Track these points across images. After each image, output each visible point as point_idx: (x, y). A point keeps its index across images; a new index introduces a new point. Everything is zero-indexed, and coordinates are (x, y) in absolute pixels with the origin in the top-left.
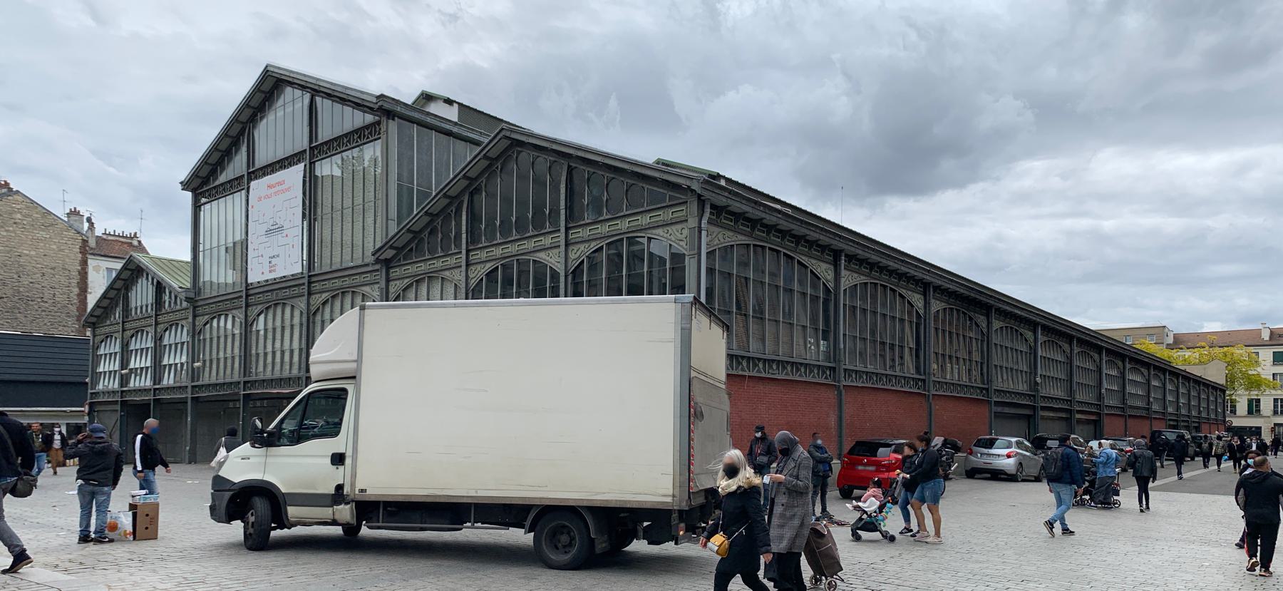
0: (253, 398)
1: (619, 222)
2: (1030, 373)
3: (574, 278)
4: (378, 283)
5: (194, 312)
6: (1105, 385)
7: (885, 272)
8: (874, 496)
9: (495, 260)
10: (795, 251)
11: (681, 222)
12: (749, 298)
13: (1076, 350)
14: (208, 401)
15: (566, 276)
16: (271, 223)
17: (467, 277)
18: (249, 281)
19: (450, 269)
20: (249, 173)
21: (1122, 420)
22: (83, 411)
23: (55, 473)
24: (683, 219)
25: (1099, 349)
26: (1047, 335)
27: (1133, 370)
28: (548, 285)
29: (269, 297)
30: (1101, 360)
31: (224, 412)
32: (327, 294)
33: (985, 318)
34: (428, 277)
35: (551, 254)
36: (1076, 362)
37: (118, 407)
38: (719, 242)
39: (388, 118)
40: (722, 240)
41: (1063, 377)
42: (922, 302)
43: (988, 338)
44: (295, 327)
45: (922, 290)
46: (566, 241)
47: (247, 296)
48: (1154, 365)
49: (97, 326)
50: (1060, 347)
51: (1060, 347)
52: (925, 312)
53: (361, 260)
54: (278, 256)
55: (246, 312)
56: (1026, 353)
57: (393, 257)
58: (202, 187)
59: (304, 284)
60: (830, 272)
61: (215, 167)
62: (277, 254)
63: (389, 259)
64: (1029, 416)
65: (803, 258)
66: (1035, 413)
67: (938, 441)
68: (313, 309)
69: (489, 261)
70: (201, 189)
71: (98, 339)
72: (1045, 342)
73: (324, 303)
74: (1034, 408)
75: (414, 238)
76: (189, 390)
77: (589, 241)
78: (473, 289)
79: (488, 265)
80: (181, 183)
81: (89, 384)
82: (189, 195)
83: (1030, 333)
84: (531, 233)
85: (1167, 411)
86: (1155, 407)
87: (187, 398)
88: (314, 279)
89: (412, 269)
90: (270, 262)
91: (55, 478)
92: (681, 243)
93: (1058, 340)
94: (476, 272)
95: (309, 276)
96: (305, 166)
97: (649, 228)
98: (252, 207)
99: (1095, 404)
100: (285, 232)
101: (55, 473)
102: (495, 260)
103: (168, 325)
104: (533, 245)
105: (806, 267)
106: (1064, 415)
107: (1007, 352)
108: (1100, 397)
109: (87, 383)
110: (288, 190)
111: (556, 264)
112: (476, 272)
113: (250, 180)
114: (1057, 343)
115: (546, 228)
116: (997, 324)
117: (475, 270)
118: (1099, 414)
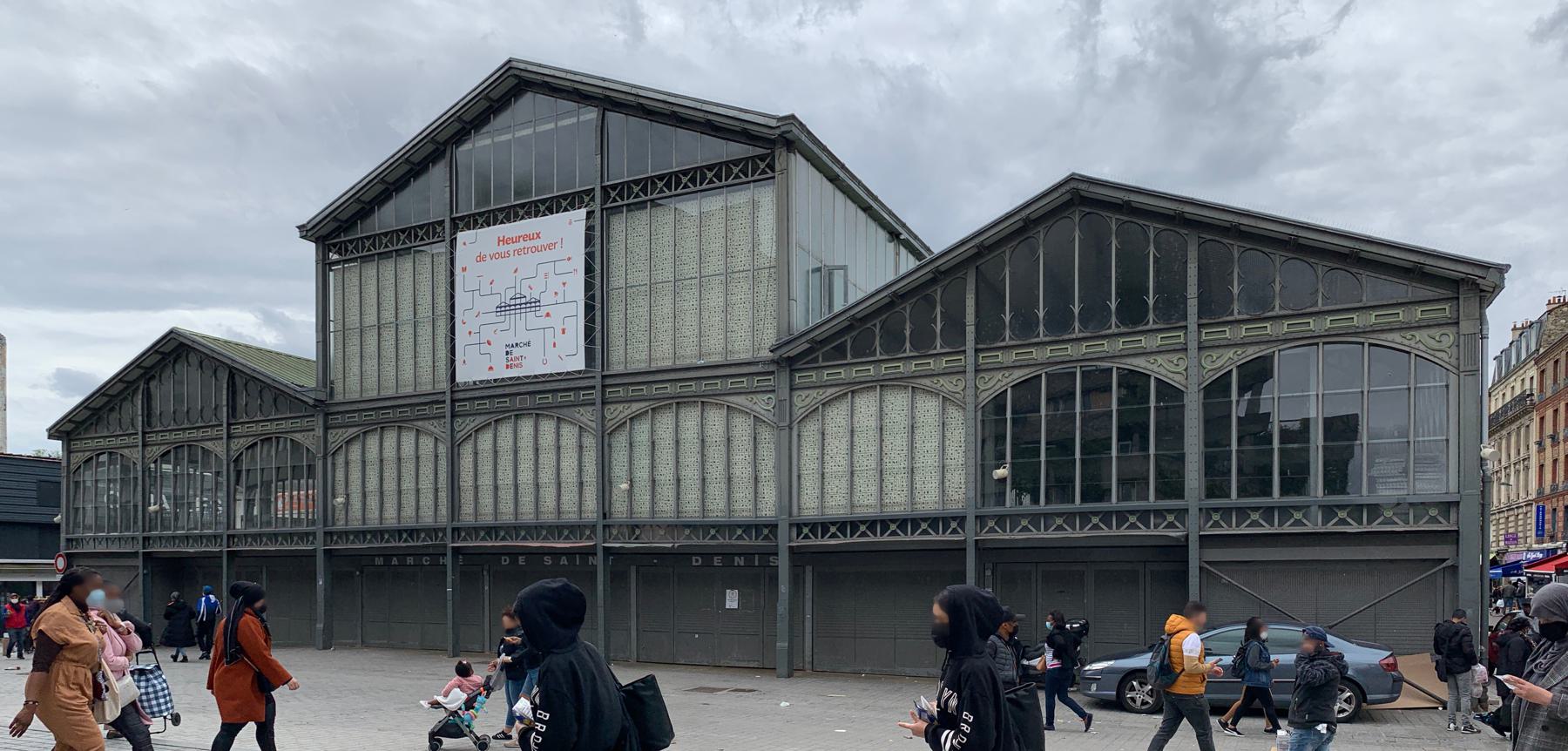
0: (464, 552)
1: (1033, 350)
3: (236, 466)
4: (313, 430)
5: (325, 422)
8: (459, 687)
9: (167, 443)
11: (958, 373)
14: (355, 557)
15: (228, 465)
16: (511, 293)
17: (453, 429)
18: (458, 379)
19: (128, 447)
20: (453, 220)
22: (53, 564)
24: (961, 369)
28: (1152, 404)
29: (99, 444)
31: (362, 572)
32: (355, 429)
34: (881, 386)
35: (755, 400)
37: (139, 562)
38: (961, 399)
39: (789, 151)
44: (352, 465)
46: (452, 413)
47: (453, 401)
49: (72, 437)
53: (395, 390)
54: (528, 344)
55: (452, 425)
57: (72, 430)
58: (338, 236)
59: (593, 387)
61: (368, 207)
62: (526, 341)
63: (792, 358)
68: (610, 425)
69: (164, 444)
70: (334, 238)
71: (78, 458)
73: (349, 442)
75: (93, 415)
76: (320, 536)
77: (1243, 344)
78: (983, 407)
79: (163, 448)
80: (300, 228)
81: (63, 526)
82: (310, 248)
84: (1114, 330)
87: (315, 550)
88: (609, 381)
89: (92, 444)
90: (507, 353)
91: (21, 661)
92: (957, 395)
94: (463, 425)
95: (604, 377)
96: (590, 215)
97: (1374, 332)
98: (464, 269)
100: (544, 311)
102: (167, 443)
103: (257, 440)
104: (1286, 330)
109: (58, 526)
110: (551, 246)
111: (442, 434)
112: (463, 425)
113: (455, 228)
115: (1110, 327)
117: (336, 435)
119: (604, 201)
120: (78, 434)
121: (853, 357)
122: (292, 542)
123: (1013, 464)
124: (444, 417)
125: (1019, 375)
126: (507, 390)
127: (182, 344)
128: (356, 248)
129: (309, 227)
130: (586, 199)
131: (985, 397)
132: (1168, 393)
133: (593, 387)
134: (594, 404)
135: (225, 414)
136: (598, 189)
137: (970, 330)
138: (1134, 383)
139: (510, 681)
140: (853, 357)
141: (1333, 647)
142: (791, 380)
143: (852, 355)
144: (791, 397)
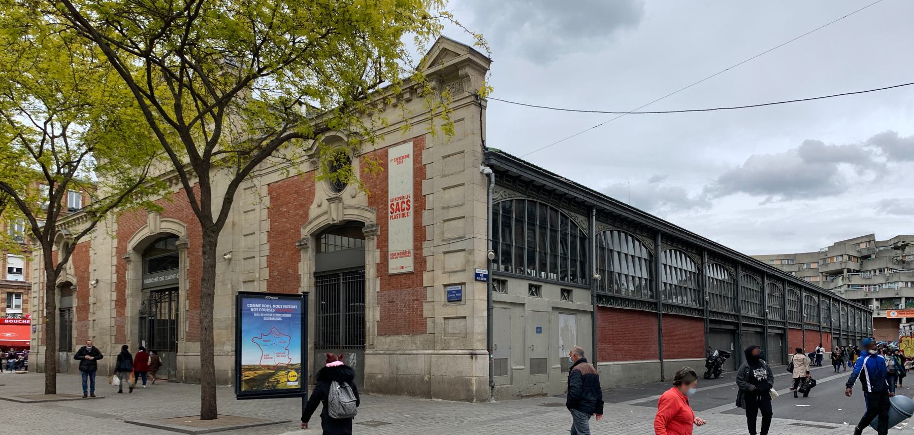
2: (699, 291)
6: (788, 307)
7: (625, 222)
10: (558, 207)
12: (567, 250)
13: (767, 282)
21: (654, 321)
23: (51, 389)
25: (762, 274)
26: (769, 280)
27: (791, 291)
30: (763, 282)
33: (586, 219)
36: (787, 297)
40: (504, 197)
41: (758, 303)
42: (701, 261)
43: (656, 258)
45: (585, 212)
48: (822, 294)
50: (755, 280)
51: (755, 280)
52: (589, 232)
56: (731, 284)
60: (584, 222)
64: (837, 338)
65: (565, 211)
66: (764, 330)
67: (716, 353)
72: (744, 275)
74: (737, 325)
83: (733, 269)
85: (740, 313)
86: (824, 324)
93: (725, 264)
99: (733, 315)
101: (51, 389)
105: (567, 218)
106: (759, 330)
107: (724, 284)
108: (764, 314)
114: (753, 277)
116: (804, 294)
118: (784, 329)
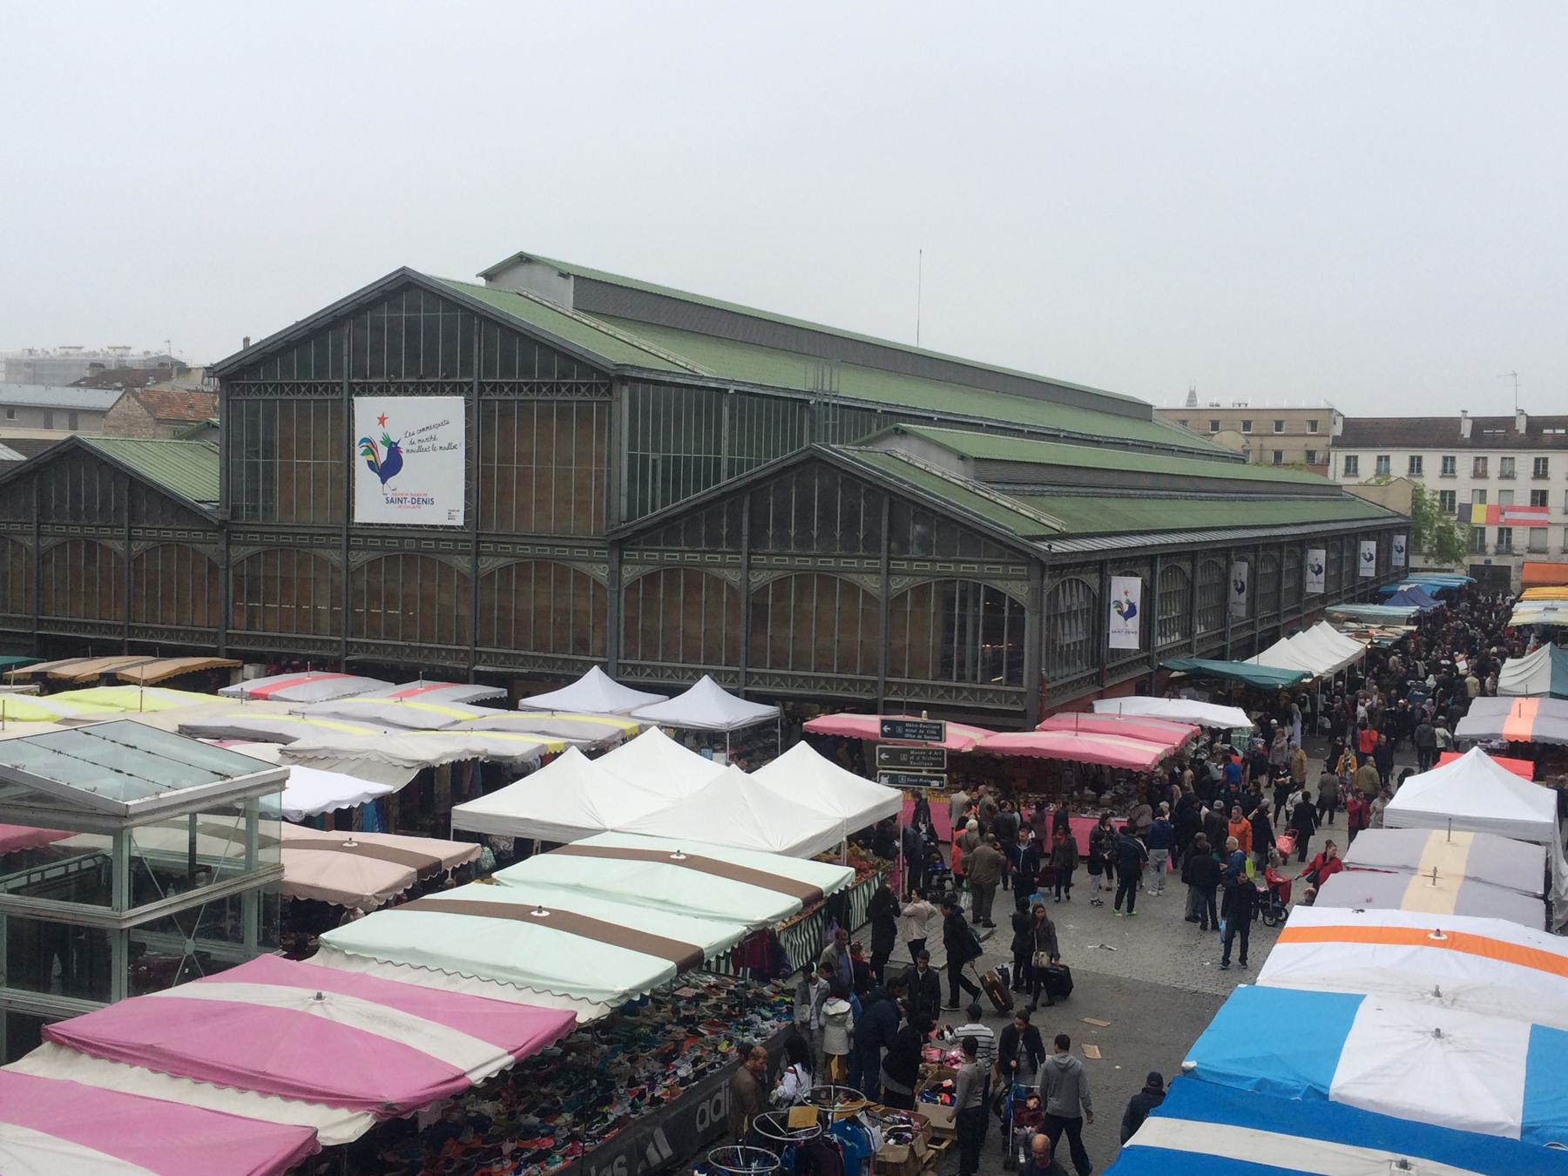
47: (348, 536)
119: (480, 394)
120: (633, 544)
121: (962, 554)
122: (100, 630)
123: (1008, 673)
124: (340, 548)
125: (777, 574)
126: (530, 541)
127: (77, 447)
128: (259, 391)
129: (217, 369)
130: (466, 389)
131: (754, 587)
132: (1017, 610)
133: (340, 536)
134: (340, 548)
135: (126, 519)
136: (476, 384)
137: (745, 538)
138: (995, 596)
139: (757, 1009)
140: (962, 554)
141: (700, 740)
142: (621, 556)
143: (864, 547)
144: (620, 568)
